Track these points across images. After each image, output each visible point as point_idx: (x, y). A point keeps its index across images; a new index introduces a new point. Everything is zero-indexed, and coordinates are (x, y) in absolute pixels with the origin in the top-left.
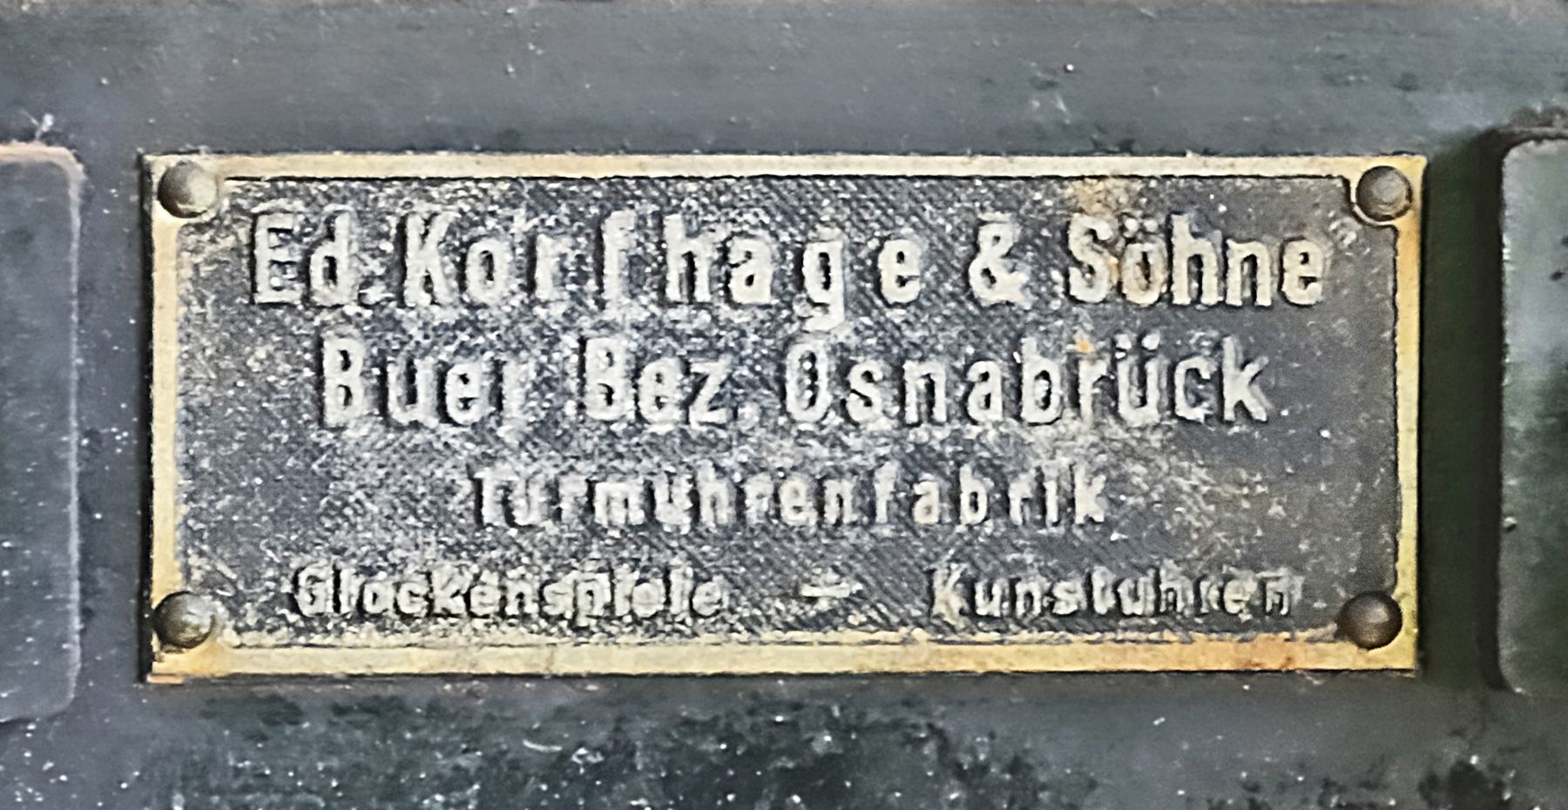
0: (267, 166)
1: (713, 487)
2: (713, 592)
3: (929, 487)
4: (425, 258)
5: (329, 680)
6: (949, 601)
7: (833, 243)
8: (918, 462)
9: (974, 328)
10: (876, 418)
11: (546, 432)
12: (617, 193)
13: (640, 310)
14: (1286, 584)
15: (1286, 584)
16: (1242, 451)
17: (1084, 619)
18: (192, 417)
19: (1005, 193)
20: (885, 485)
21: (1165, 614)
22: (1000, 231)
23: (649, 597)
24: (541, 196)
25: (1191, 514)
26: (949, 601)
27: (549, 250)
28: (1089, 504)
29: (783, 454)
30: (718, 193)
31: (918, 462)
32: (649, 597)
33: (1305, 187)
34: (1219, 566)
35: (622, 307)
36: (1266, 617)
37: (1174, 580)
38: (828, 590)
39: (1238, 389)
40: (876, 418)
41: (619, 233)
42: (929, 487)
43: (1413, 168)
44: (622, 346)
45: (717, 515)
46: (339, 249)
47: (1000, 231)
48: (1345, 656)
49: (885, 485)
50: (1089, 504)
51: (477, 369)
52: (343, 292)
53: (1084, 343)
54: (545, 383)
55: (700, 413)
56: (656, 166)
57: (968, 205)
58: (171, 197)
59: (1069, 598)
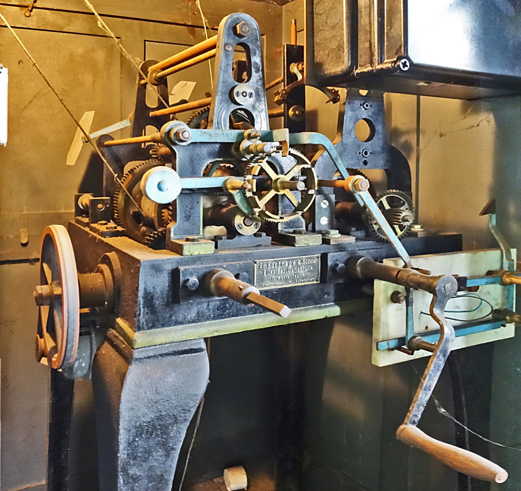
0: (261, 261)
1: (284, 277)
2: (284, 283)
3: (295, 275)
4: (269, 265)
5: (171, 259)
6: (296, 282)
7: (291, 262)
8: (295, 274)
9: (124, 346)
10: (293, 272)
11: (275, 275)
12: (279, 260)
13: (281, 267)
14: (313, 278)
15: (313, 278)
16: (312, 272)
17: (304, 282)
18: (257, 276)
19: (299, 258)
20: (293, 276)
21: (307, 281)
22: (299, 261)
23: (281, 283)
24: (275, 261)
25: (309, 275)
26: (296, 282)
27: (276, 264)
28: (304, 276)
29: (288, 274)
30: (285, 260)
31: (295, 274)
32: (281, 283)
33: (245, 292)
34: (310, 278)
35: (280, 267)
36: (313, 281)
37: (308, 279)
38: (290, 282)
39: (311, 268)
40: (293, 272)
41: (280, 263)
42: (295, 275)
43: (320, 255)
44: (280, 269)
45: (285, 278)
46: (265, 265)
47: (299, 261)
48: (316, 282)
49: (293, 276)
50: (304, 276)
51: (272, 271)
52: (265, 268)
53: (303, 266)
54: (275, 272)
55: (284, 273)
56: (281, 259)
57: (212, 312)
58: (256, 263)
59: (303, 281)
